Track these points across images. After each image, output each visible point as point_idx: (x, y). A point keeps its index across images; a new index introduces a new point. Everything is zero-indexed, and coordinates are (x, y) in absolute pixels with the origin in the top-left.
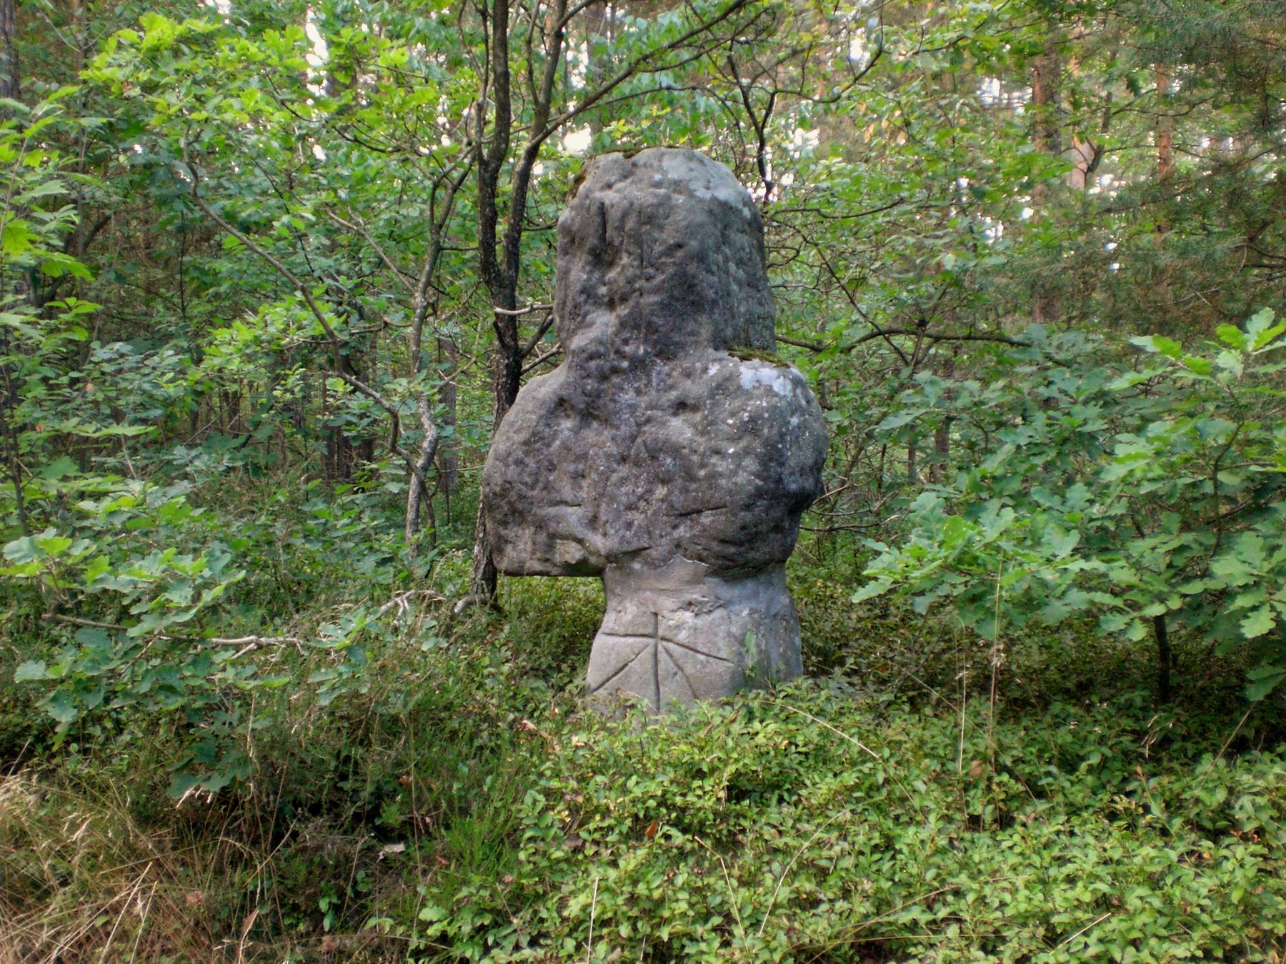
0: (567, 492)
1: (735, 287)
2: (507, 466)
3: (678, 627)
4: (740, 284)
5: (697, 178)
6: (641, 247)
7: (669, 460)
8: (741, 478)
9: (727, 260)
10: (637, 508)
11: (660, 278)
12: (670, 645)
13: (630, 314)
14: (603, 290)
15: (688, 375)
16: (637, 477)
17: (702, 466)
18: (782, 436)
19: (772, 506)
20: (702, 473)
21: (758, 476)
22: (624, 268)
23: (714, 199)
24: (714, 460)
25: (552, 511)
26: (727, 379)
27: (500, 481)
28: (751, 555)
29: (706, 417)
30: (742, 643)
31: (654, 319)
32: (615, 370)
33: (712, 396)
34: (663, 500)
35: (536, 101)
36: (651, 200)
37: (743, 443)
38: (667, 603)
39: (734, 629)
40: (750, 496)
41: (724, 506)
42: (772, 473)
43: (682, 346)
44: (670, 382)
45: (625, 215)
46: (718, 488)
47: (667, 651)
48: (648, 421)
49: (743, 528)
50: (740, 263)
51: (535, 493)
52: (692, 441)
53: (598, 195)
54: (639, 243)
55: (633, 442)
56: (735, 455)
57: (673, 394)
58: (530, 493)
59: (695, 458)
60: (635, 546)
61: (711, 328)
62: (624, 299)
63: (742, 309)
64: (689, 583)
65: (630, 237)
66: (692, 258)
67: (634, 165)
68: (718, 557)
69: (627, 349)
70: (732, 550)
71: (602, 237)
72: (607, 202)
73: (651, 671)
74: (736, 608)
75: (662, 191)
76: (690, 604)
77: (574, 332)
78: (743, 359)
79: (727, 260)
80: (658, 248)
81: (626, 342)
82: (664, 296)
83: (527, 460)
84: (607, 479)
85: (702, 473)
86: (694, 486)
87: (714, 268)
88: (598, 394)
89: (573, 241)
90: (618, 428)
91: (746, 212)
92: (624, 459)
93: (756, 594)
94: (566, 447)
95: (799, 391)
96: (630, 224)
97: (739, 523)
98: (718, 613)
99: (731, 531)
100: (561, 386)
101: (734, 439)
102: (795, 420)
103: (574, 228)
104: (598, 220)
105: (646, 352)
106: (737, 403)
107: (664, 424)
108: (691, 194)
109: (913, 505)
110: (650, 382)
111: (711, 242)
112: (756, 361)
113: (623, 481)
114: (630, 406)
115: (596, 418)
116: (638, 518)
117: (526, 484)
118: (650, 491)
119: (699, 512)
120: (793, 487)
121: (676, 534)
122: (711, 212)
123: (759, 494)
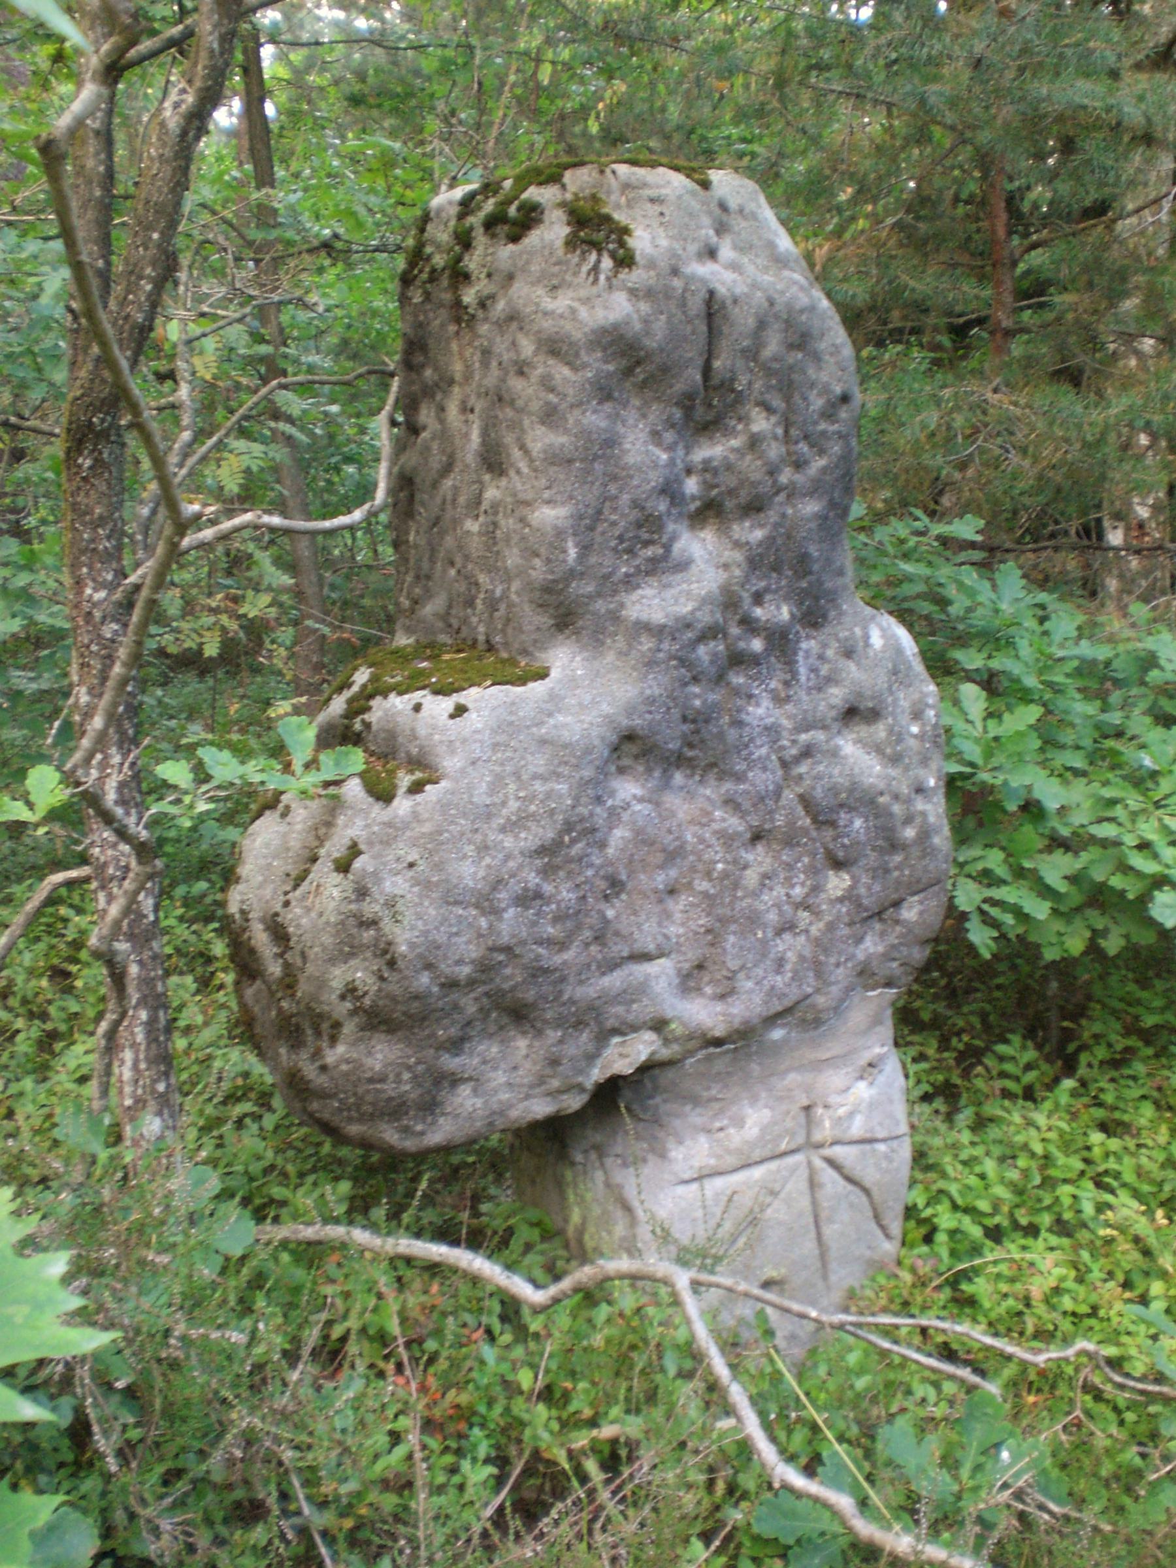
0: (647, 935)
2: (496, 912)
6: (788, 399)
7: (858, 823)
13: (770, 540)
16: (789, 867)
17: (908, 820)
20: (910, 833)
22: (754, 442)
25: (613, 981)
27: (474, 952)
34: (841, 900)
44: (824, 670)
47: (831, 1162)
48: (807, 752)
51: (568, 955)
57: (837, 695)
58: (558, 959)
62: (754, 508)
65: (769, 372)
69: (758, 612)
72: (722, 290)
77: (630, 583)
81: (758, 599)
83: (548, 888)
84: (736, 886)
89: (628, 372)
90: (740, 778)
92: (757, 837)
94: (642, 838)
100: (630, 711)
103: (651, 343)
110: (794, 674)
116: (791, 947)
117: (549, 942)
119: (897, 904)
121: (860, 953)
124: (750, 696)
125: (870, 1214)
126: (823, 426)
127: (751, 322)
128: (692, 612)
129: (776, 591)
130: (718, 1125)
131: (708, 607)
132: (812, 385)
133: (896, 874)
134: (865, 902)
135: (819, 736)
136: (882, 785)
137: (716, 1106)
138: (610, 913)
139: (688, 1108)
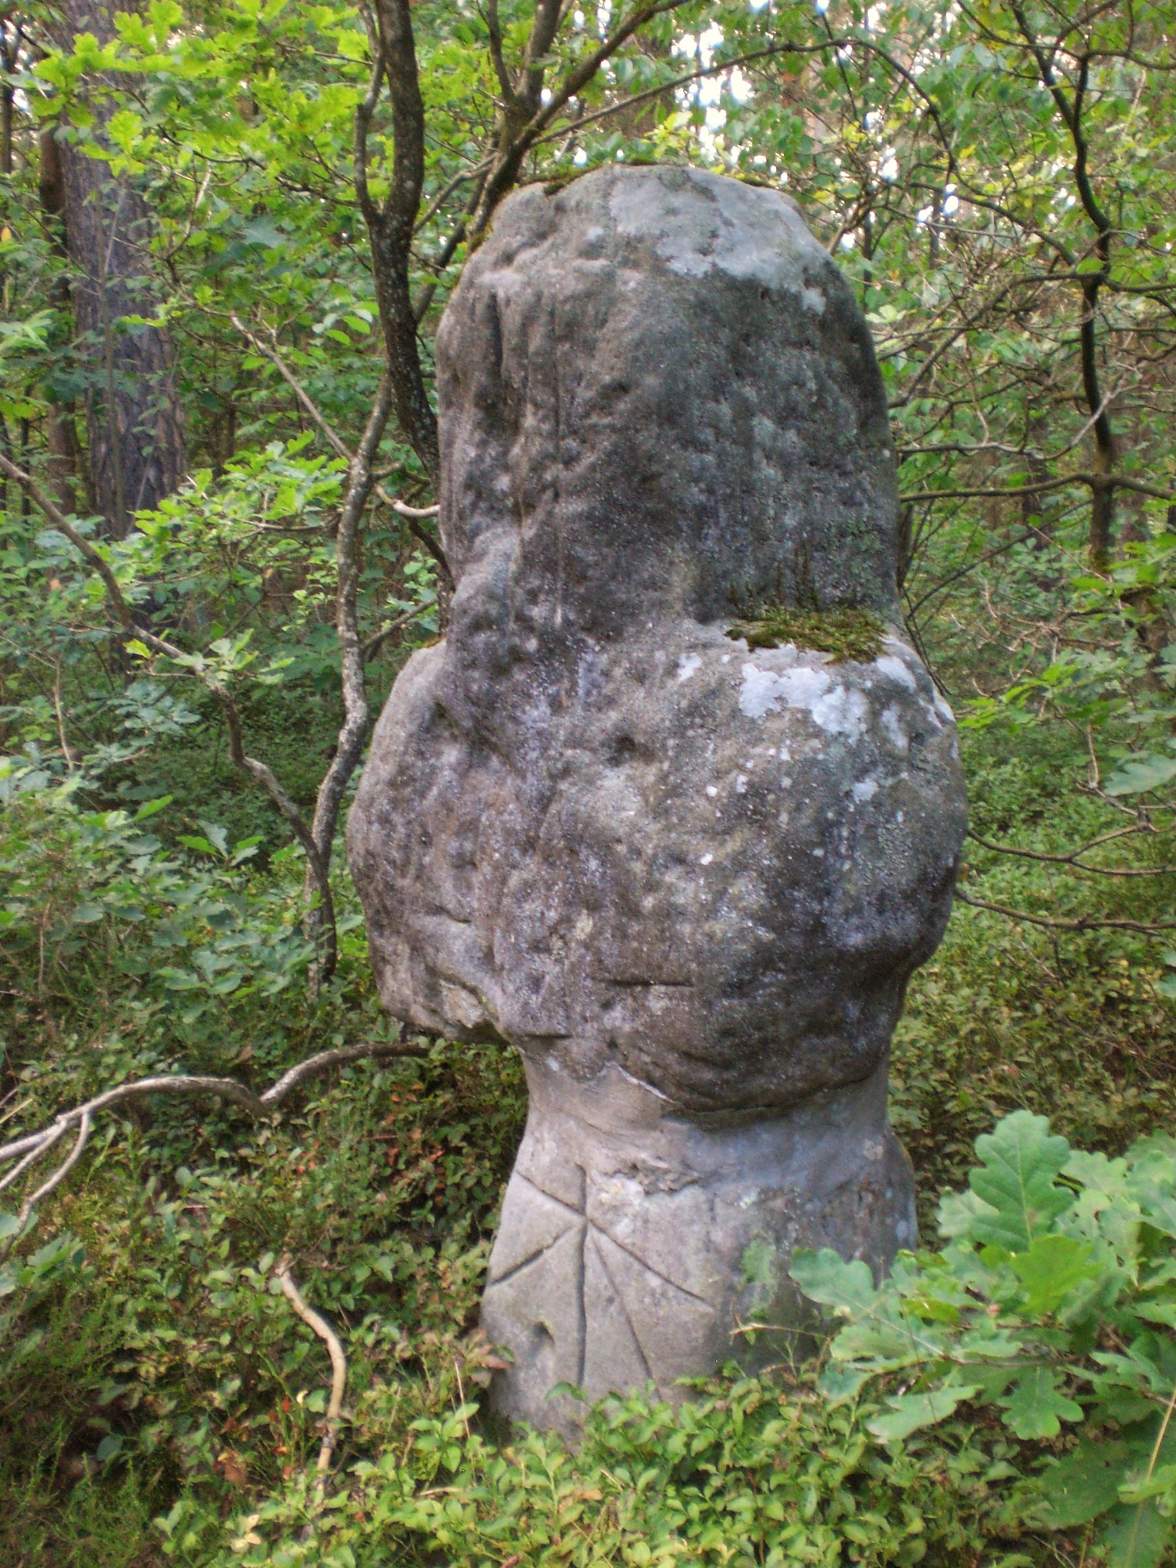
0: (448, 894)
1: (770, 472)
3: (616, 1209)
4: (786, 463)
5: (680, 231)
7: (593, 864)
8: (725, 924)
9: (745, 411)
10: (548, 950)
11: (589, 458)
12: (604, 1240)
14: (503, 482)
15: (640, 677)
17: (651, 887)
18: (825, 831)
19: (798, 984)
20: (649, 902)
21: (762, 919)
23: (718, 273)
24: (671, 877)
26: (713, 693)
28: (758, 1083)
29: (663, 778)
30: (736, 1266)
31: (579, 550)
32: (518, 656)
33: (679, 731)
35: (507, 93)
36: (573, 285)
37: (733, 844)
38: (599, 1158)
39: (718, 1236)
40: (742, 967)
41: (687, 982)
42: (797, 913)
43: (631, 611)
44: (608, 689)
45: (528, 320)
46: (675, 940)
49: (726, 1033)
50: (786, 416)
52: (635, 827)
53: (487, 278)
54: (552, 383)
55: (544, 809)
56: (716, 866)
59: (638, 867)
60: (542, 1028)
61: (694, 571)
63: (790, 520)
64: (633, 1123)
66: (647, 417)
67: (560, 208)
68: (680, 1086)
70: (708, 1075)
71: (495, 370)
73: (573, 1282)
74: (728, 1189)
75: (598, 264)
78: (756, 643)
79: (745, 411)
80: (585, 394)
81: (533, 597)
82: (596, 501)
84: (504, 881)
85: (649, 902)
86: (635, 928)
87: (708, 435)
88: (490, 703)
91: (814, 299)
92: (529, 845)
93: (783, 1157)
95: (890, 717)
96: (536, 342)
97: (717, 1021)
98: (689, 1197)
99: (700, 1039)
101: (716, 833)
102: (866, 789)
104: (486, 332)
105: (567, 622)
106: (729, 749)
107: (591, 781)
108: (659, 267)
109: (983, 1143)
110: (574, 684)
111: (695, 376)
112: (788, 649)
113: (526, 891)
114: (540, 733)
115: (494, 748)
116: (547, 966)
117: (393, 863)
118: (567, 921)
120: (855, 939)
122: (702, 307)
123: (765, 958)
124: (530, 696)
125: (632, 1348)
126: (594, 419)
127: (518, 319)
128: (470, 598)
129: (551, 591)
131: (480, 598)
132: (579, 378)
133: (635, 944)
134: (608, 962)
135: (585, 757)
136: (622, 832)
138: (427, 860)
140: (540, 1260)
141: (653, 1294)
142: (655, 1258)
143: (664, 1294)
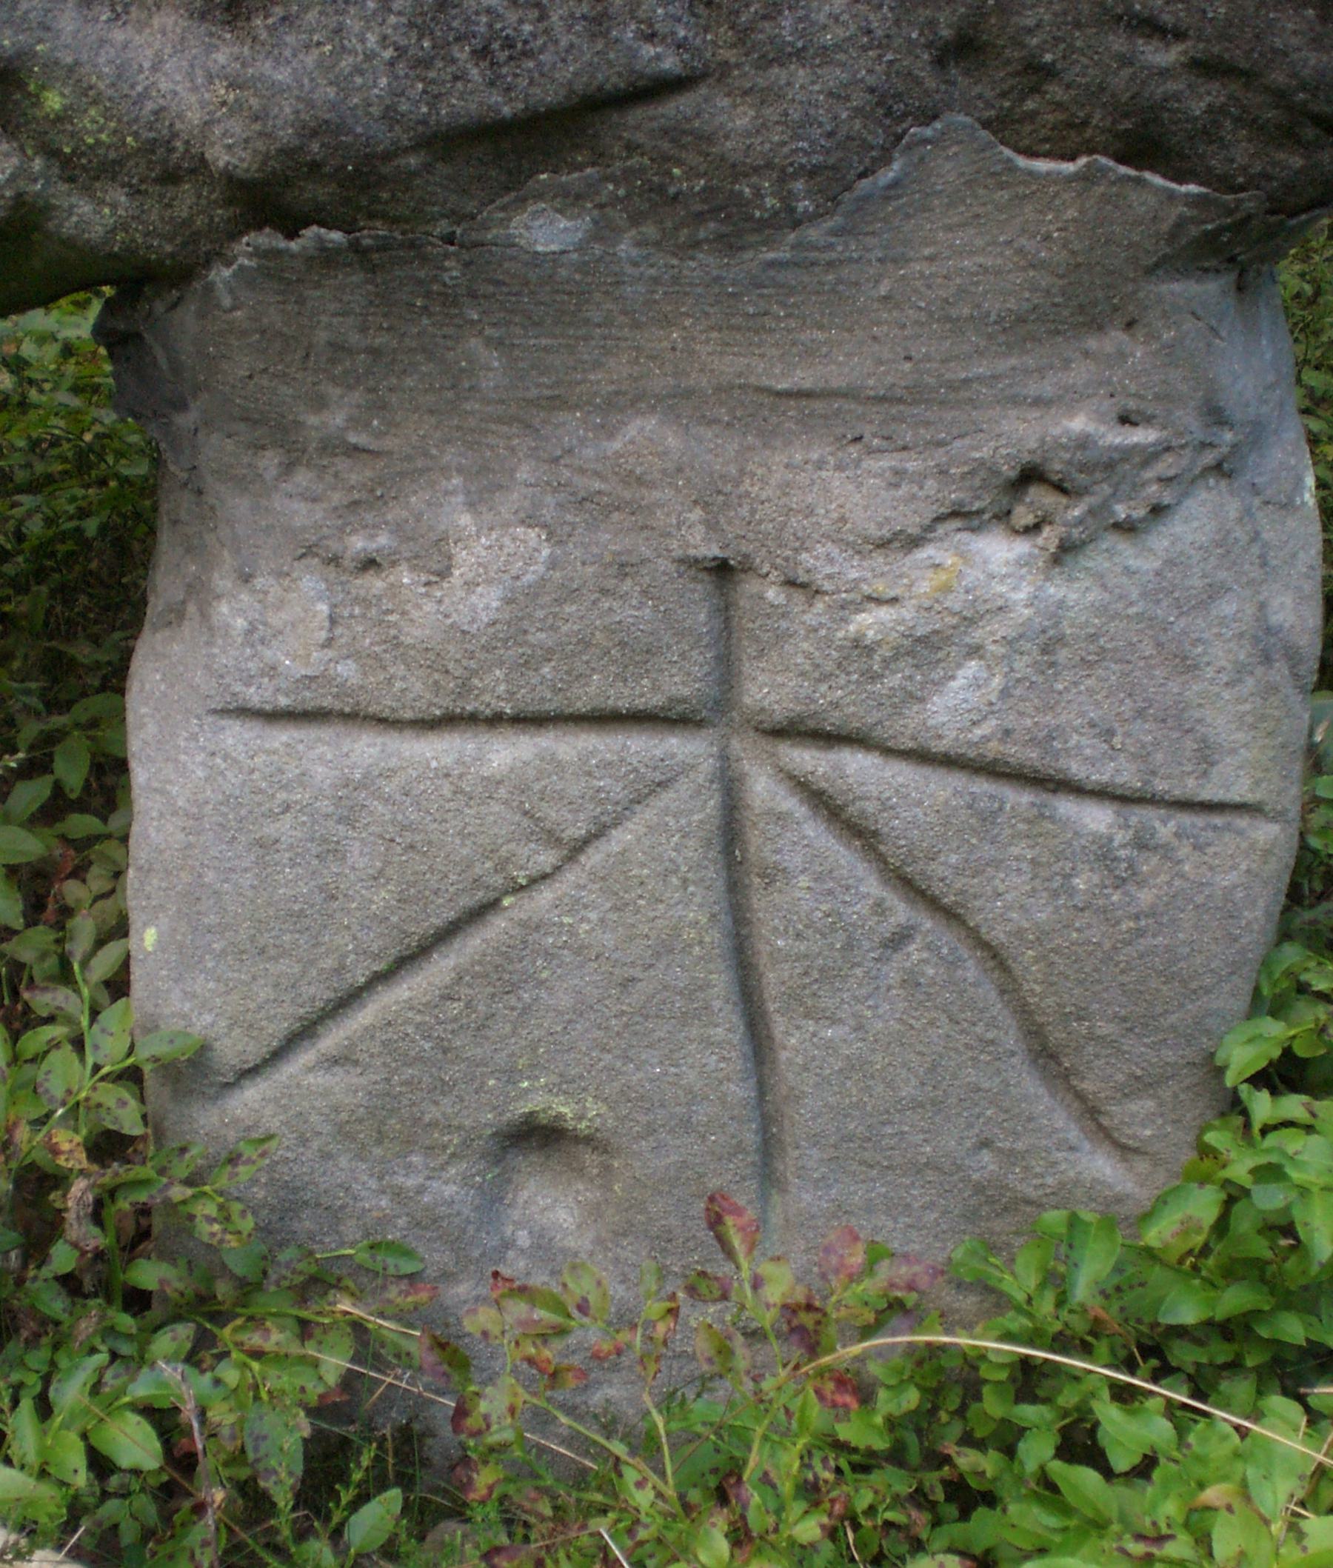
76: (1030, 476)
125: (1011, 1038)
130: (358, 544)
137: (357, 474)
139: (270, 462)
140: (497, 926)
141: (1103, 854)
142: (1089, 745)
143: (1141, 844)
